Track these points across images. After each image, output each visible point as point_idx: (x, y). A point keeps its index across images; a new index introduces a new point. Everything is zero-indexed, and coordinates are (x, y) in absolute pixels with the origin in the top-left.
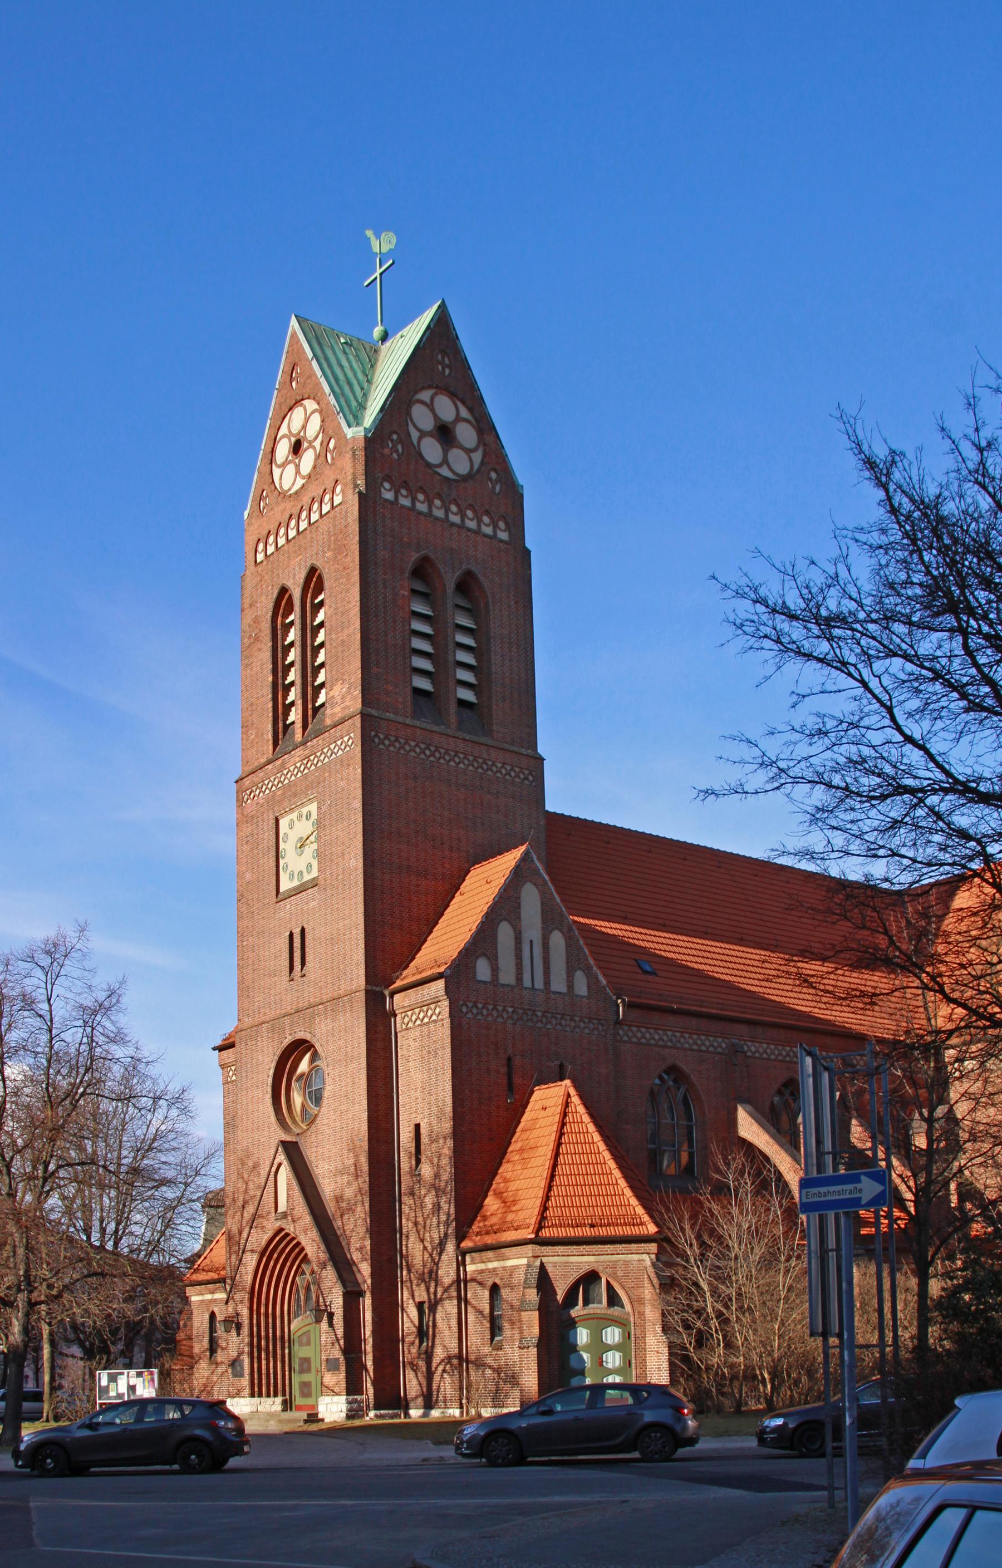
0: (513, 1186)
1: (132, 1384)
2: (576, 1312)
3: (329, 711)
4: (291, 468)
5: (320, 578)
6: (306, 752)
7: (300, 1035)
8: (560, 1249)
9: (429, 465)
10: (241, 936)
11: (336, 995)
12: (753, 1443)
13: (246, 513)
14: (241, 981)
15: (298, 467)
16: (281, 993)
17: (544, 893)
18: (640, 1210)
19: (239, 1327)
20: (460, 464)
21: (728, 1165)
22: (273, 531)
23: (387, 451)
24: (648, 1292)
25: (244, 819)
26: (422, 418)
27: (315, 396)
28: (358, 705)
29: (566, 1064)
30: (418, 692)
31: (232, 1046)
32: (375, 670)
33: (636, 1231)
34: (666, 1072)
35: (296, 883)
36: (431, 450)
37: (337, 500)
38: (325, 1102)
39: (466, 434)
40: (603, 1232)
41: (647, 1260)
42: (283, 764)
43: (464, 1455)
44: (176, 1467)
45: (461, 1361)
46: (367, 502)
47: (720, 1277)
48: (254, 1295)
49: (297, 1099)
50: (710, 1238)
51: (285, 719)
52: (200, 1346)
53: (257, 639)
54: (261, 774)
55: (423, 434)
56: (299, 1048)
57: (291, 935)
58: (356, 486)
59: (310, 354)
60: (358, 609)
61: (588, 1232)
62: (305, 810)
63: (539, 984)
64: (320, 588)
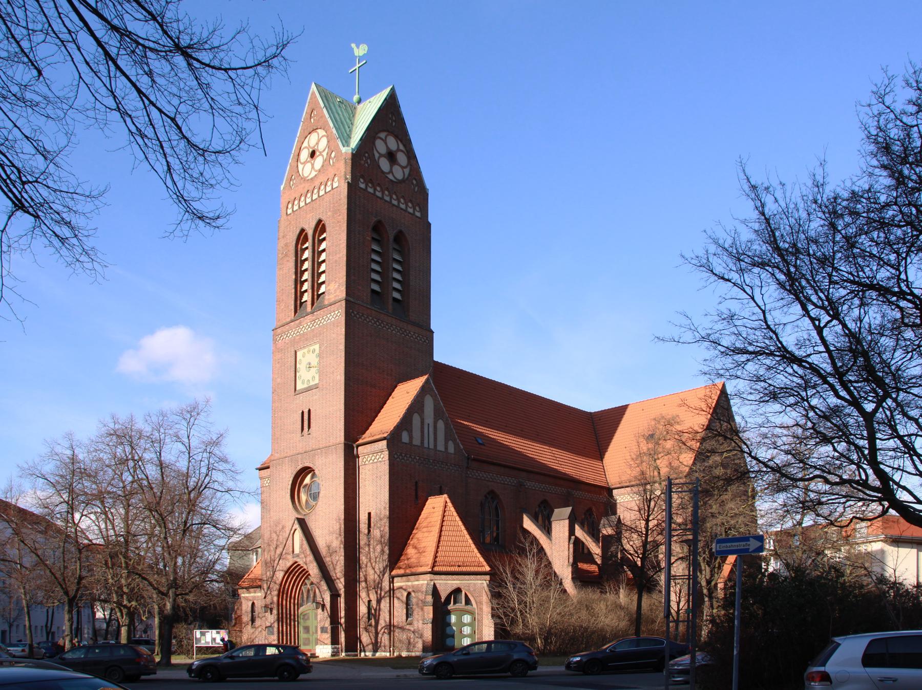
0: (423, 545)
1: (212, 637)
2: (451, 607)
3: (327, 297)
4: (309, 166)
5: (324, 225)
7: (307, 465)
8: (443, 577)
9: (383, 172)
10: (274, 411)
11: (327, 445)
12: (563, 669)
13: (282, 187)
14: (273, 435)
15: (313, 165)
16: (296, 442)
17: (435, 400)
18: (482, 559)
19: (271, 610)
20: (399, 173)
21: (525, 539)
22: (298, 198)
23: (362, 162)
24: (485, 598)
25: (278, 350)
26: (381, 147)
27: (325, 127)
28: (344, 295)
30: (373, 291)
31: (268, 468)
32: (353, 277)
33: (480, 569)
34: (488, 493)
35: (305, 386)
36: (384, 164)
37: (335, 185)
38: (320, 499)
39: (402, 158)
40: (464, 569)
41: (485, 584)
42: (300, 323)
43: (424, 674)
44: (276, 678)
45: (390, 627)
46: (352, 188)
47: (521, 593)
48: (281, 592)
49: (304, 497)
50: (517, 575)
51: (301, 299)
52: (246, 618)
53: (286, 255)
54: (287, 327)
55: (381, 155)
56: (305, 471)
57: (303, 413)
58: (346, 179)
59: (322, 105)
60: (345, 244)
61: (457, 569)
62: (312, 348)
63: (432, 446)
64: (323, 230)
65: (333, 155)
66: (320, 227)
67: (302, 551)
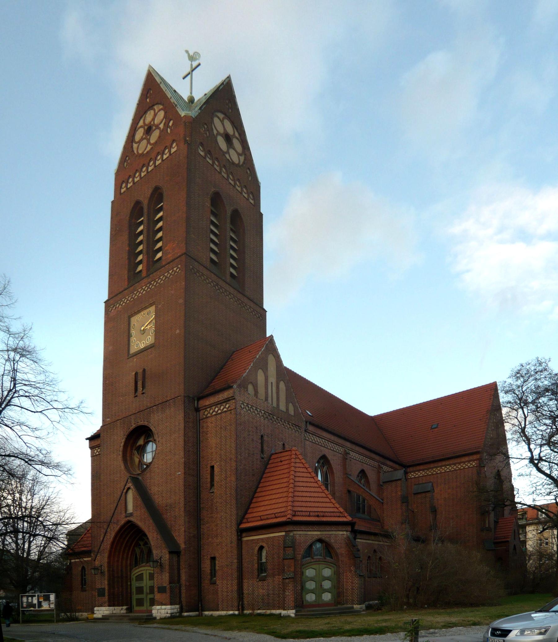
4: (145, 142)
6: (149, 280)
7: (141, 423)
29: (286, 444)
34: (320, 458)
57: (136, 374)
63: (275, 405)
64: (160, 198)
65: (170, 124)
66: (157, 195)
67: (135, 506)
